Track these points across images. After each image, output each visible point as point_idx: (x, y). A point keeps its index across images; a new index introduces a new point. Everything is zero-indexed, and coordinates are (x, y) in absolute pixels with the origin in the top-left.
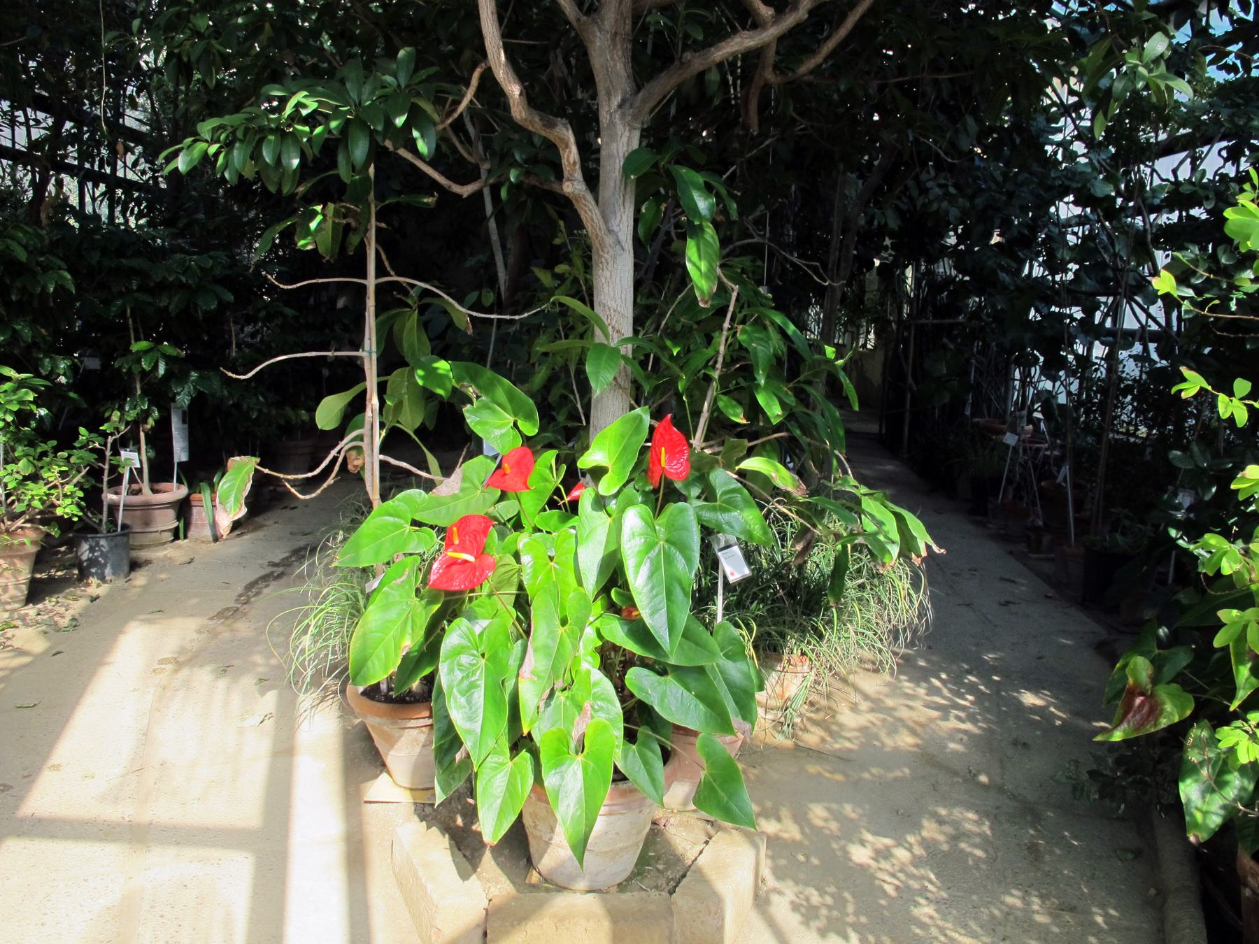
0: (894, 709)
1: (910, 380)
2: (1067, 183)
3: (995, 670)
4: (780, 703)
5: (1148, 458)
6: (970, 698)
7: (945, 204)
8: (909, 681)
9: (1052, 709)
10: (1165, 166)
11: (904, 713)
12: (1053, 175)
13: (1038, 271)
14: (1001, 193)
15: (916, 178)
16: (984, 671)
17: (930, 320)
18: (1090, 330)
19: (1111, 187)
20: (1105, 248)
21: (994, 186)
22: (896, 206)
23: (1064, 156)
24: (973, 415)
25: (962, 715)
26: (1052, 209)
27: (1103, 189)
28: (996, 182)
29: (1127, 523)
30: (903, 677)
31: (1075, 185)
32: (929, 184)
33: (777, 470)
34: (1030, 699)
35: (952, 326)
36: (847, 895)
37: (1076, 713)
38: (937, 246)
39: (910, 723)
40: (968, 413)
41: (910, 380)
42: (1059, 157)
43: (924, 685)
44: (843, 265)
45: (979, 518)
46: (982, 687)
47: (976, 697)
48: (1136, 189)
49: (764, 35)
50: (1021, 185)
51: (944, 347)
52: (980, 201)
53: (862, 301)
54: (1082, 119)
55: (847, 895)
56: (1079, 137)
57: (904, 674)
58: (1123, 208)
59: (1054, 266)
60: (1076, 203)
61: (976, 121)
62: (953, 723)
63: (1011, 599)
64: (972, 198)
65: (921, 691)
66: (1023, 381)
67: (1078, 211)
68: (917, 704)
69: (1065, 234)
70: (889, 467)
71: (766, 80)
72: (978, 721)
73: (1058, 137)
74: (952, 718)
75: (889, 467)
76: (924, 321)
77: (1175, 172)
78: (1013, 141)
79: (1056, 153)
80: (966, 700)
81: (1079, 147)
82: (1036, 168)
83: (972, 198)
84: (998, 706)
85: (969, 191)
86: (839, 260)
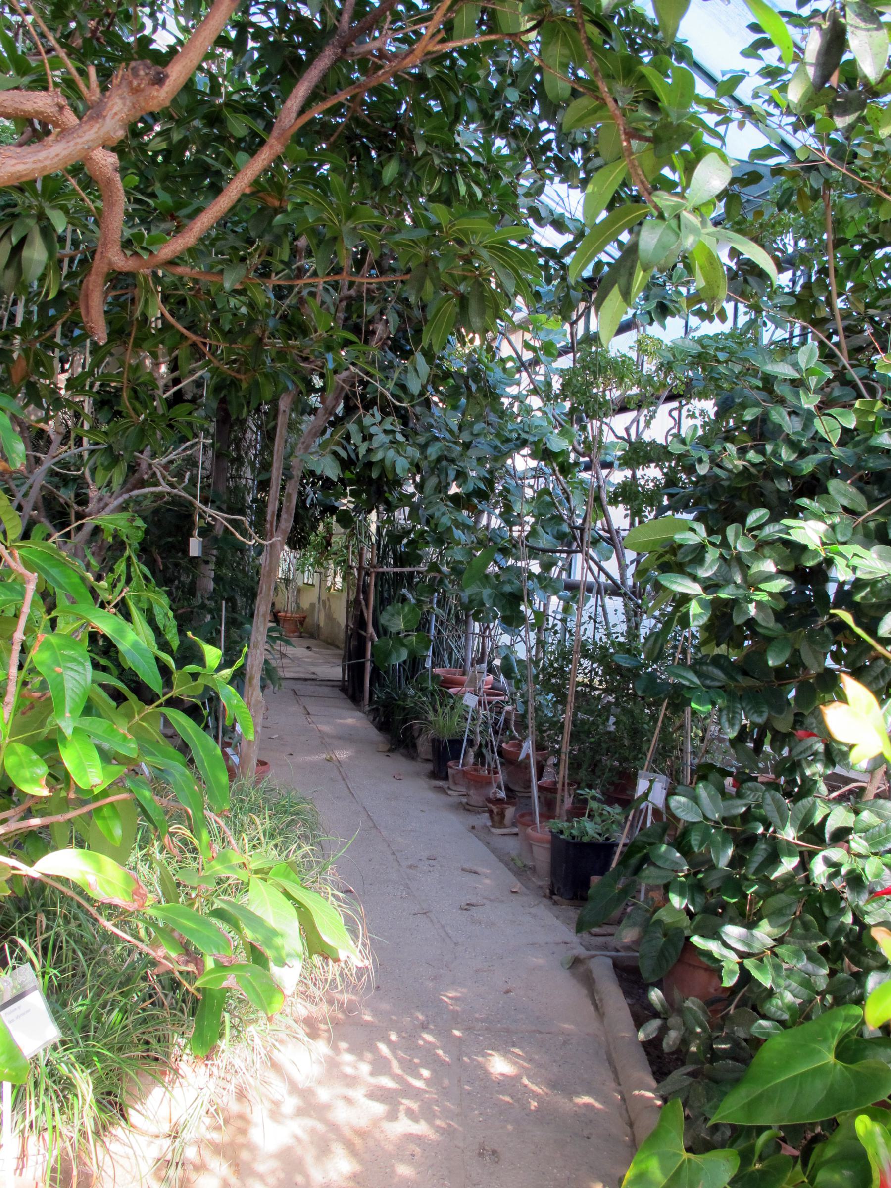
0: (327, 1107)
1: (371, 629)
2: (524, 435)
3: (456, 1019)
4: (166, 1128)
5: (612, 728)
6: (426, 1073)
7: (391, 454)
8: (350, 1051)
9: (525, 1081)
10: (620, 422)
11: (342, 1114)
12: (510, 427)
13: (496, 523)
14: (455, 443)
15: (359, 422)
16: (440, 1019)
17: (389, 569)
18: (545, 583)
19: (566, 442)
20: (560, 502)
21: (448, 436)
22: (335, 454)
23: (520, 410)
24: (433, 666)
25: (415, 1106)
26: (509, 462)
27: (557, 443)
28: (451, 431)
29: (593, 805)
30: (343, 1045)
31: (531, 439)
32: (373, 430)
33: (99, 869)
34: (500, 1065)
35: (411, 575)
36: (523, 247)
37: (554, 1085)
38: (396, 494)
39: (347, 1132)
40: (428, 664)
41: (371, 629)
42: (515, 409)
43: (369, 1056)
44: (284, 516)
45: (440, 783)
46: (440, 1052)
47: (434, 1071)
48: (591, 446)
49: (42, 155)
50: (477, 435)
51: (404, 599)
52: (433, 452)
53: (329, 544)
54: (537, 374)
55: (523, 247)
56: (535, 391)
57: (344, 1038)
58: (576, 464)
59: (508, 517)
60: (533, 456)
61: (619, 667)
62: (404, 1126)
63: (474, 901)
64: (423, 448)
65: (365, 1068)
66: (482, 635)
67: (533, 464)
68: (358, 1094)
69: (523, 486)
70: (350, 721)
71: (110, 263)
72: (435, 1116)
73: (513, 390)
74: (402, 1115)
75: (350, 721)
76: (385, 569)
77: (627, 430)
78: (469, 388)
79: (511, 405)
80: (419, 1076)
81: (535, 402)
82: (493, 418)
83: (423, 448)
84: (463, 1085)
85: (421, 440)
86: (280, 510)
